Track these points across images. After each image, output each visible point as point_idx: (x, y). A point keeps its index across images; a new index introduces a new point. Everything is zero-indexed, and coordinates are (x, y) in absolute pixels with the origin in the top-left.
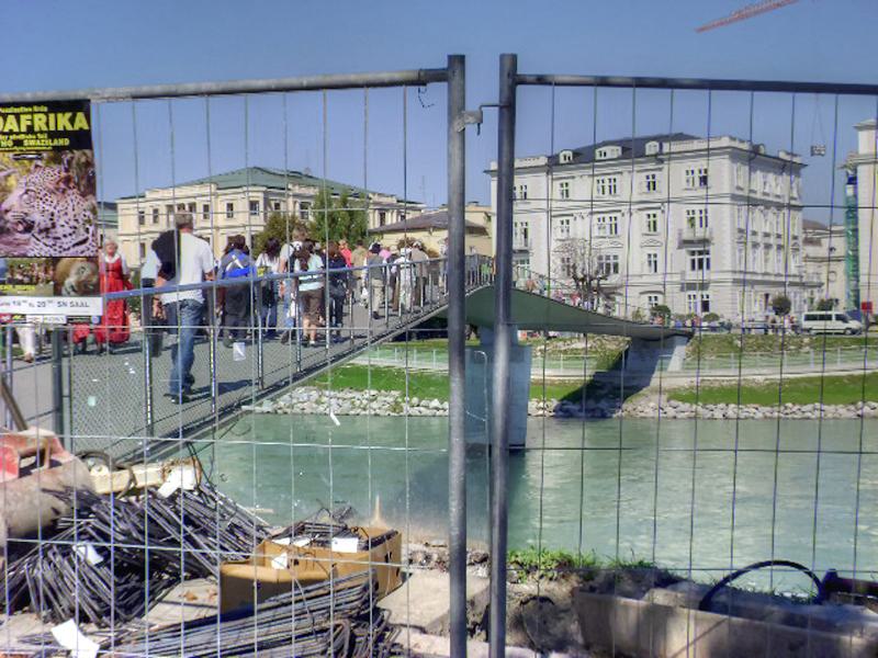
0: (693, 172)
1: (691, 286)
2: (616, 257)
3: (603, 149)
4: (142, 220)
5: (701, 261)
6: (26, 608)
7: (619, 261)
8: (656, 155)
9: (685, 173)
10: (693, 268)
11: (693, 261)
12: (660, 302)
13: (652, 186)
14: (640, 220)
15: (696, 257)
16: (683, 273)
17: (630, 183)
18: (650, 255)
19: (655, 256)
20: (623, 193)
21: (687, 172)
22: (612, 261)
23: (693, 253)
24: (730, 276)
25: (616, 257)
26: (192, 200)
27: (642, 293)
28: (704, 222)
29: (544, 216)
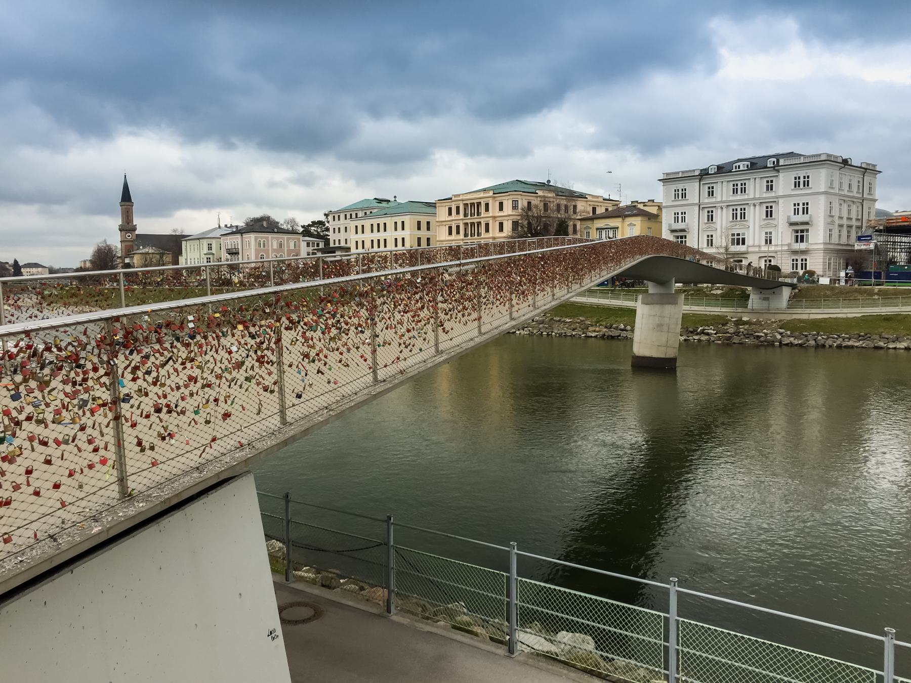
0: (678, 190)
1: (795, 252)
2: (744, 234)
3: (737, 164)
4: (450, 214)
5: (738, 239)
6: (103, 459)
7: (746, 237)
8: (774, 167)
9: (674, 191)
10: (797, 241)
11: (797, 236)
12: (772, 263)
13: (770, 188)
14: (761, 211)
15: (799, 234)
16: (727, 249)
17: (756, 188)
18: (733, 235)
19: (712, 236)
20: (718, 197)
21: (675, 190)
22: (741, 237)
23: (797, 231)
24: (822, 246)
25: (744, 234)
26: (478, 201)
27: (760, 257)
28: (806, 211)
29: (697, 208)
